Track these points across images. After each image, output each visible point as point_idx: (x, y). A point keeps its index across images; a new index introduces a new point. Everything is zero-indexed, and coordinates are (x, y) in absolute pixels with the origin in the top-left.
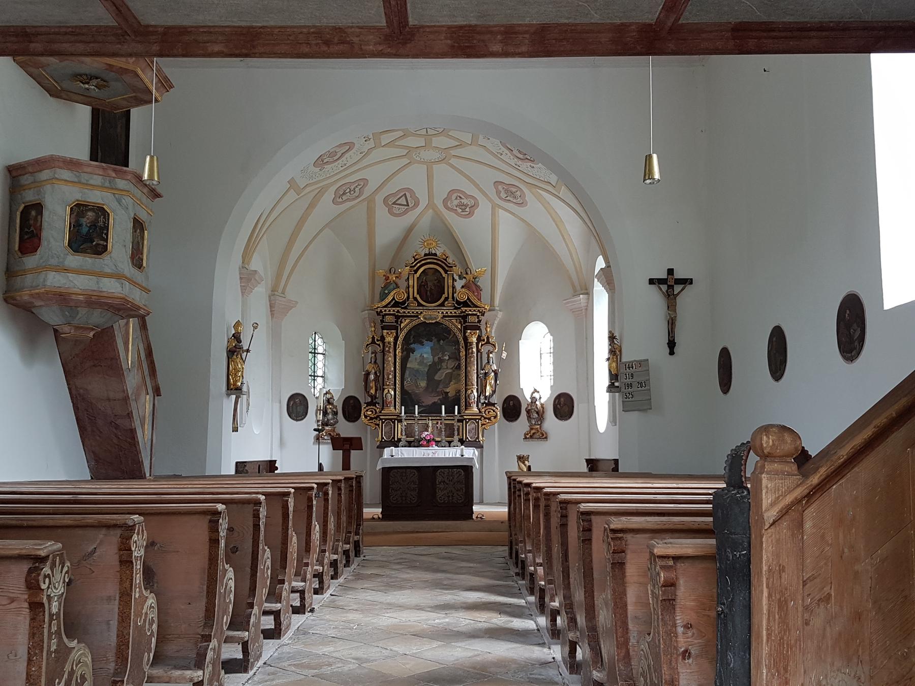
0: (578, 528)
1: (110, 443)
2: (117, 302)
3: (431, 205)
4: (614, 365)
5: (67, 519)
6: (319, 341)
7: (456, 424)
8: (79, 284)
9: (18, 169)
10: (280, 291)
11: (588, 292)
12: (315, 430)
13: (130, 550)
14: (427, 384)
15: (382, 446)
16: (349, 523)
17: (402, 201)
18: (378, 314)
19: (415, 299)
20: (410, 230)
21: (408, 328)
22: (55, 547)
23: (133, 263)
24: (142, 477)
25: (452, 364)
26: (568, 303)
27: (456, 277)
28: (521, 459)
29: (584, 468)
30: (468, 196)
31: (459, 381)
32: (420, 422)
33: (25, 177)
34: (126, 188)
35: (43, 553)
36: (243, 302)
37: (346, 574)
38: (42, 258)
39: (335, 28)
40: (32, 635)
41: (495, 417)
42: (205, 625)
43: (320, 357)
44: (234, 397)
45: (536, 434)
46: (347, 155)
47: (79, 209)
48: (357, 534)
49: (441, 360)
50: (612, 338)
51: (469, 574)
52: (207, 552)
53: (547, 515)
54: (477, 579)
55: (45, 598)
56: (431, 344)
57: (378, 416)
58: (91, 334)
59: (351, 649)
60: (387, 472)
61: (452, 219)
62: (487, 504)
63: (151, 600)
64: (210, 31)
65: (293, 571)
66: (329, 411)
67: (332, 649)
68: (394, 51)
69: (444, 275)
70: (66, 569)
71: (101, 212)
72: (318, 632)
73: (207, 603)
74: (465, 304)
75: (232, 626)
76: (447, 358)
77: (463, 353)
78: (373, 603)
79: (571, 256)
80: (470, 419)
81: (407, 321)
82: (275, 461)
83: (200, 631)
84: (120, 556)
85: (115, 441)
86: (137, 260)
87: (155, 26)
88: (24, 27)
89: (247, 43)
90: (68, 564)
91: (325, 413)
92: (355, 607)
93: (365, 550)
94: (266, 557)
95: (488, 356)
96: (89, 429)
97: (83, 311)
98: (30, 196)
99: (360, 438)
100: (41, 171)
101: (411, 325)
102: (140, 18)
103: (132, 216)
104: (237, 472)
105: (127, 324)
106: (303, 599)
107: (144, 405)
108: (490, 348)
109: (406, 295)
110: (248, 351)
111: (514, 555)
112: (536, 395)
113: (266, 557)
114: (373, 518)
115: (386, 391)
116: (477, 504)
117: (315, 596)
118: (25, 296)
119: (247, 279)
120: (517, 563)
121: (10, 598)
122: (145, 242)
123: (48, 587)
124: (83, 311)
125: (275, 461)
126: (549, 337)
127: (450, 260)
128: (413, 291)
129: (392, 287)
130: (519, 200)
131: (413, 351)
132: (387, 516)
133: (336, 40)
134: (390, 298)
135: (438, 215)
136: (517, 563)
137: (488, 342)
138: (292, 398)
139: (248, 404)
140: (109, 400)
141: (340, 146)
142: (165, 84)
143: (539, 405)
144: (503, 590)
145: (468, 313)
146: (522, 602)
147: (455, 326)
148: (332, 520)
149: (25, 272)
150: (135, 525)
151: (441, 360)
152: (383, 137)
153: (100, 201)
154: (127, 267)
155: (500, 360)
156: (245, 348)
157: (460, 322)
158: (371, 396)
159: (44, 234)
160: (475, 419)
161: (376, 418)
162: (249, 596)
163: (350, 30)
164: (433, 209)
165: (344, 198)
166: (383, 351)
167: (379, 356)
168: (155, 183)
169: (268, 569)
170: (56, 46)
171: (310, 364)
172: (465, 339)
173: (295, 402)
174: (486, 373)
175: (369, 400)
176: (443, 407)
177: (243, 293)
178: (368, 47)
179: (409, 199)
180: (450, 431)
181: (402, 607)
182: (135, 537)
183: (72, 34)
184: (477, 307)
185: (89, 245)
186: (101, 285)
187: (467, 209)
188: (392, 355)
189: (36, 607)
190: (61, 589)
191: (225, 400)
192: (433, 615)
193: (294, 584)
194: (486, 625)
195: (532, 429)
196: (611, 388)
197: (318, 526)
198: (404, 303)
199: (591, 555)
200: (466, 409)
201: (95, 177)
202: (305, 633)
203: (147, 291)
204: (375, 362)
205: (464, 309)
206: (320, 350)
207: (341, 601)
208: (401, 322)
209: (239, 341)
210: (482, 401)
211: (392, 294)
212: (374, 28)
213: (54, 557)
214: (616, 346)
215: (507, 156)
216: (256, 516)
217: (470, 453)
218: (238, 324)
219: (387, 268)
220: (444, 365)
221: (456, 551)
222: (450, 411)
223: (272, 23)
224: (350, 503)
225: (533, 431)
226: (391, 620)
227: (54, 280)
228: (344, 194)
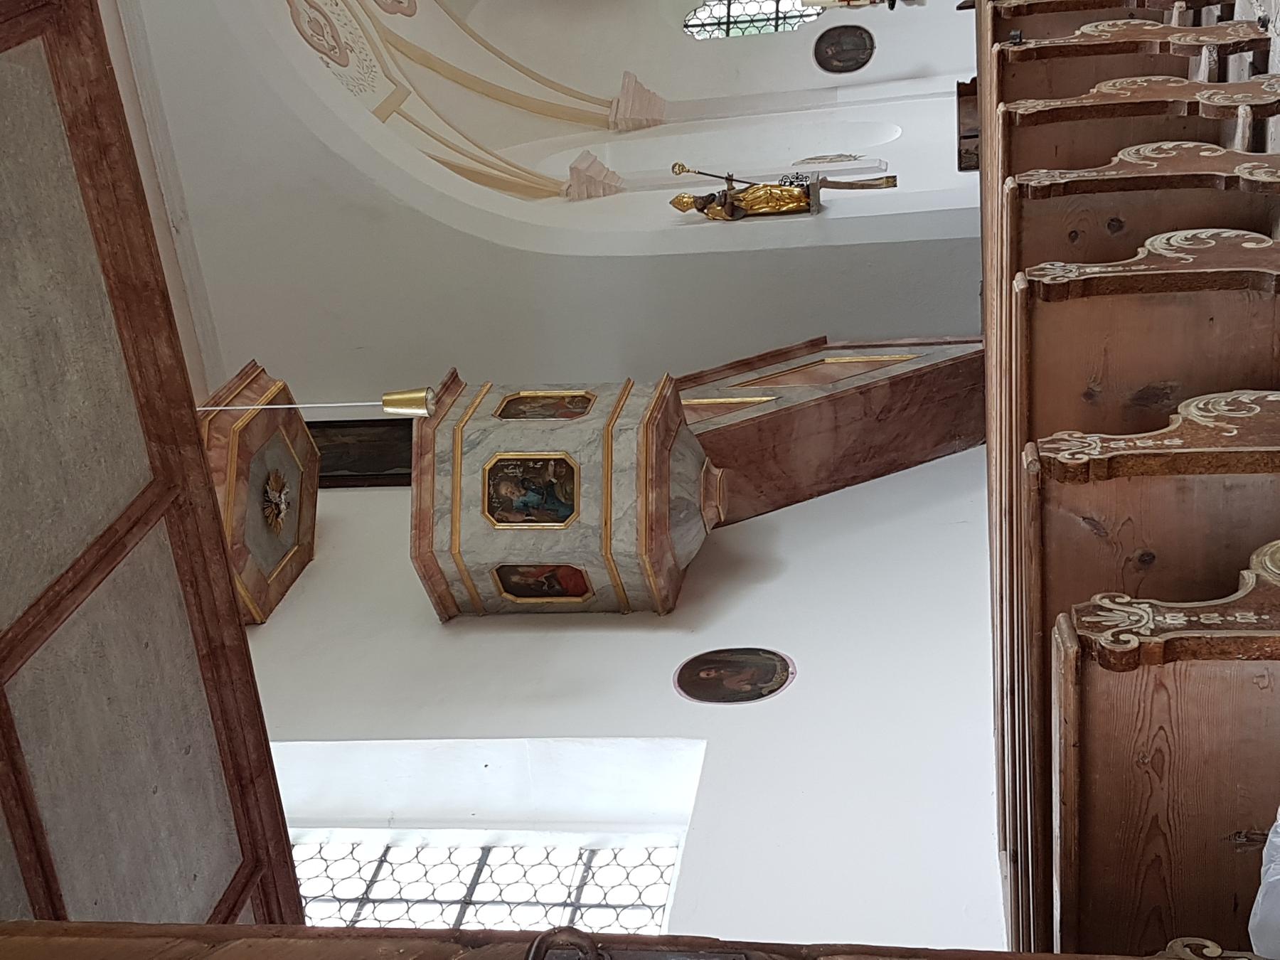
1: (920, 417)
2: (653, 438)
5: (1029, 568)
6: (703, 15)
8: (628, 501)
9: (445, 608)
10: (604, 111)
13: (1087, 464)
22: (1064, 626)
23: (582, 414)
24: (981, 357)
33: (456, 594)
34: (449, 435)
35: (1073, 648)
38: (591, 562)
39: (72, 138)
40: (1225, 654)
42: (1257, 287)
43: (736, 10)
44: (825, 194)
47: (497, 508)
55: (1157, 639)
58: (717, 472)
63: (1191, 410)
64: (137, 363)
65: (1174, 82)
68: (86, 12)
70: (1106, 603)
71: (497, 473)
73: (1211, 287)
82: (959, 85)
83: (1267, 297)
84: (1099, 478)
85: (913, 410)
86: (576, 407)
87: (151, 457)
88: (201, 658)
89: (141, 298)
90: (1097, 599)
94: (1137, 157)
96: (893, 455)
97: (676, 491)
98: (488, 586)
100: (441, 572)
102: (143, 484)
103: (497, 420)
104: (976, 168)
105: (693, 408)
106: (1238, 47)
107: (847, 368)
110: (729, 179)
117: (1237, 17)
118: (659, 584)
119: (589, 184)
121: (1156, 690)
122: (541, 394)
123: (1137, 634)
124: (676, 491)
125: (959, 85)
133: (93, 133)
138: (825, 62)
139: (841, 157)
140: (836, 428)
142: (252, 376)
149: (618, 586)
150: (1040, 459)
153: (479, 476)
154: (592, 422)
159: (549, 561)
162: (1213, 186)
163: (68, 107)
168: (430, 395)
169: (1159, 150)
170: (223, 608)
171: (754, 31)
173: (834, 56)
177: (618, 190)
178: (92, 68)
182: (1064, 457)
183: (195, 584)
185: (557, 489)
186: (627, 464)
189: (1171, 652)
190: (1144, 610)
191: (831, 214)
193: (1202, 75)
197: (1086, 29)
201: (437, 487)
203: (628, 385)
206: (720, 11)
209: (712, 198)
212: (51, 59)
213: (1082, 625)
218: (678, 203)
223: (94, 257)
227: (627, 540)
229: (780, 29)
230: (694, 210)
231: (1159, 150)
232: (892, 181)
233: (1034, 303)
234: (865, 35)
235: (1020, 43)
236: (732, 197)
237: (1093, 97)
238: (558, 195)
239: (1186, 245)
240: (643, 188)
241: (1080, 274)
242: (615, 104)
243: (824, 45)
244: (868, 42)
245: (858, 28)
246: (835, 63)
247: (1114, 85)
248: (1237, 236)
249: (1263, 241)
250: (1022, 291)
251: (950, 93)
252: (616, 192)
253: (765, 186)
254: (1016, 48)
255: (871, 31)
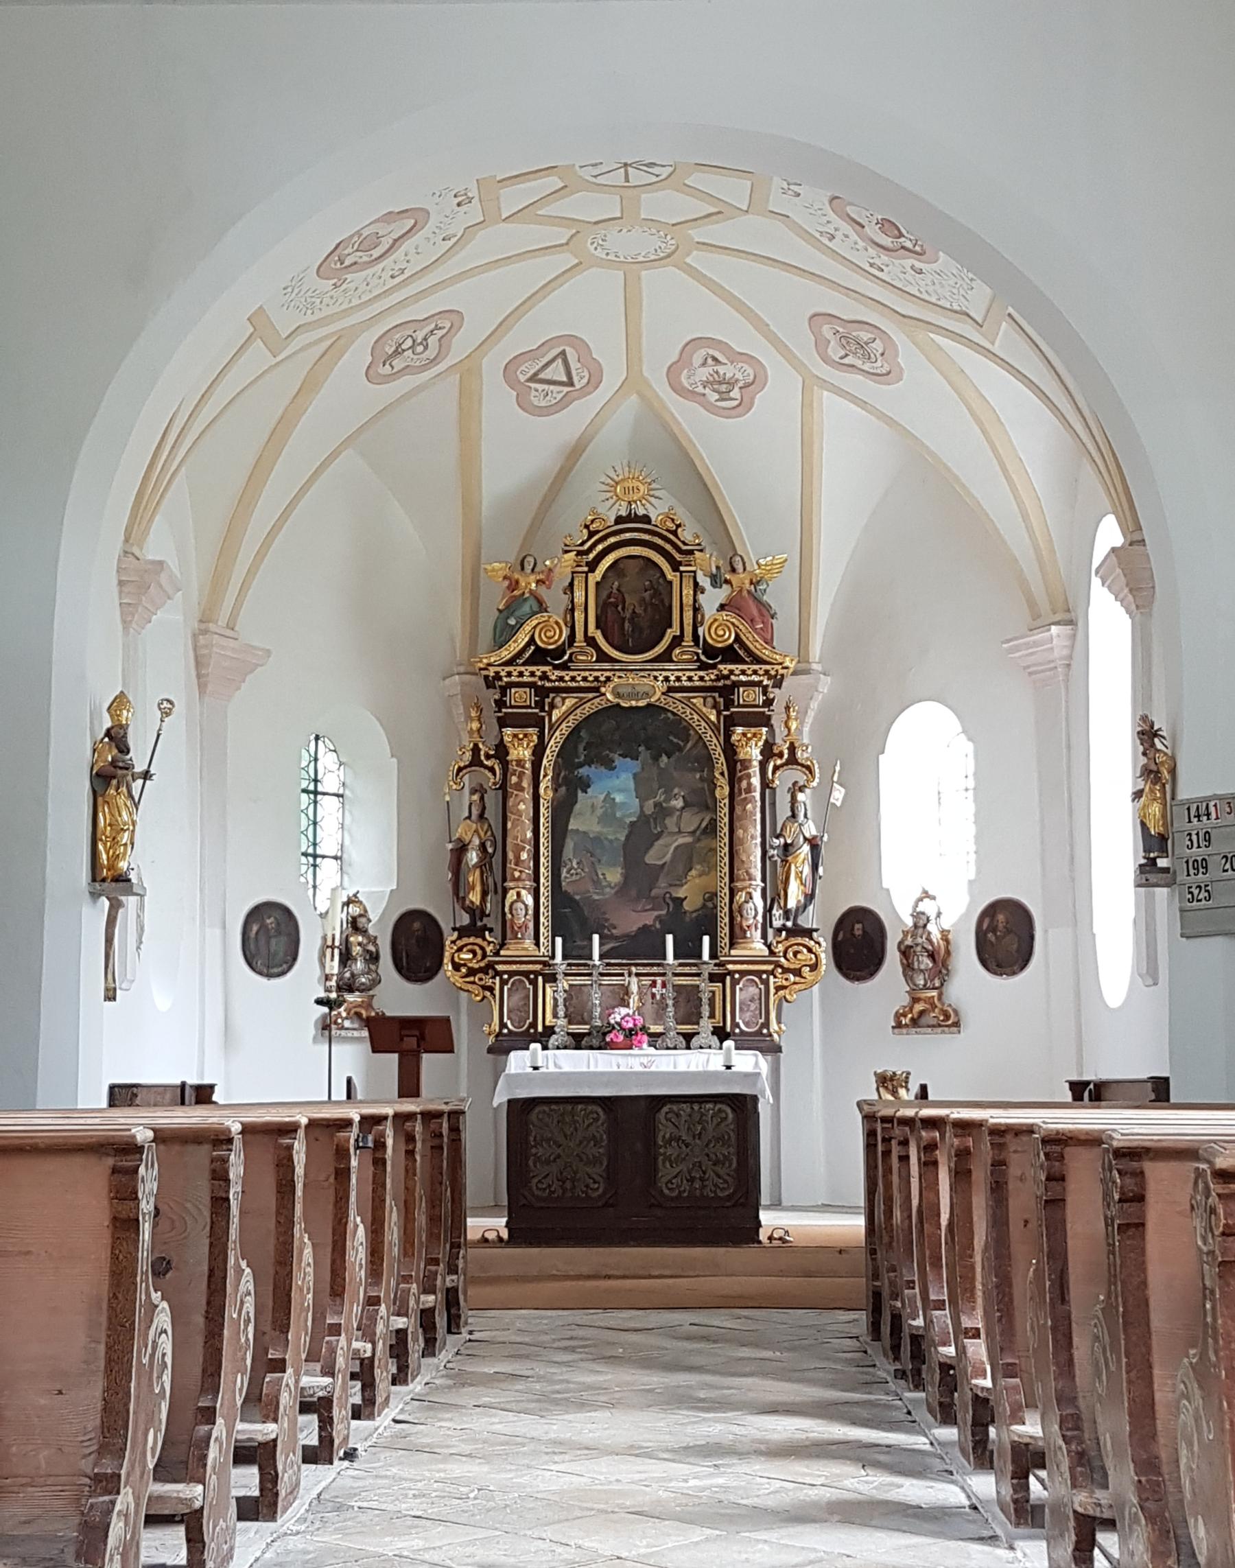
0: (1107, 1195)
3: (633, 381)
4: (1156, 809)
6: (328, 760)
7: (706, 987)
11: (1070, 615)
12: (319, 1002)
14: (626, 877)
15: (503, 1046)
16: (433, 1236)
17: (555, 373)
18: (489, 683)
19: (591, 641)
20: (576, 452)
21: (571, 722)
25: (692, 821)
26: (1017, 649)
27: (704, 581)
28: (886, 1081)
29: (1068, 1097)
30: (737, 357)
31: (712, 867)
32: (606, 981)
36: (126, 647)
37: (428, 1373)
41: (814, 967)
42: (103, 1450)
43: (328, 806)
45: (928, 1014)
46: (408, 245)
48: (452, 1269)
49: (662, 811)
50: (1147, 735)
51: (764, 1374)
52: (105, 1255)
53: (998, 1189)
54: (788, 1386)
56: (635, 766)
57: (491, 966)
59: (472, 1543)
60: (520, 1110)
61: (690, 419)
62: (794, 1208)
66: (356, 950)
67: (418, 1543)
69: (670, 575)
72: (374, 1505)
73: (107, 1390)
74: (729, 654)
75: (163, 1472)
76: (679, 803)
77: (722, 791)
78: (513, 1440)
79: (1025, 517)
80: (743, 973)
81: (569, 702)
82: (211, 1087)
83: (86, 1465)
91: (346, 958)
92: (467, 1449)
93: (473, 1320)
94: (244, 1288)
95: (794, 800)
99: (447, 1020)
101: (579, 715)
106: (326, 1423)
108: (799, 776)
109: (566, 632)
110: (146, 775)
111: (886, 1329)
112: (927, 907)
113: (244, 1288)
114: (485, 1240)
115: (511, 896)
116: (768, 1208)
117: (355, 1423)
119: (138, 584)
120: (896, 1348)
125: (211, 1087)
126: (969, 747)
127: (686, 535)
128: (587, 622)
129: (526, 608)
130: (880, 366)
131: (585, 785)
132: (519, 1234)
134: (522, 639)
135: (653, 414)
136: (896, 1348)
137: (793, 760)
138: (258, 913)
141: (389, 217)
143: (936, 936)
144: (865, 1413)
145: (736, 675)
146: (919, 1442)
147: (702, 714)
148: (393, 1217)
151: (662, 811)
152: (505, 192)
155: (826, 809)
156: (139, 768)
157: (715, 706)
158: (471, 910)
160: (758, 973)
161: (484, 970)
162: (203, 1391)
164: (641, 396)
165: (398, 363)
166: (503, 786)
167: (492, 799)
169: (248, 1321)
172: (730, 751)
173: (263, 926)
174: (786, 846)
175: (465, 919)
176: (670, 938)
177: (126, 624)
179: (574, 365)
180: (689, 1006)
181: (592, 1450)
184: (759, 660)
187: (732, 391)
188: (527, 796)
191: (87, 910)
192: (682, 1469)
194: (828, 1494)
195: (915, 1000)
196: (1148, 872)
197: (361, 1229)
198: (559, 652)
199: (1142, 1267)
200: (732, 945)
202: (339, 1508)
204: (481, 816)
205: (725, 668)
206: (330, 783)
207: (425, 1434)
208: (552, 706)
210: (777, 923)
211: (527, 628)
214: (1160, 758)
215: (848, 242)
216: (220, 1176)
217: (747, 1061)
218: (120, 702)
219: (513, 557)
220: (670, 822)
221: (720, 1320)
222: (689, 950)
224: (434, 1183)
225: (919, 1007)
226: (568, 1478)
228: (398, 352)
229: (304, 859)
230: (108, 723)
231: (248, 1321)
232: (110, 996)
233: (108, 1155)
234: (285, 966)
235: (357, 1147)
236: (125, 776)
237: (302, 1237)
238: (127, 540)
239: (158, 1354)
240: (126, 658)
241: (144, 1214)
242: (229, 633)
243: (278, 914)
244: (276, 970)
245: (295, 959)
246: (255, 928)
247: (309, 1264)
248: (160, 1421)
249: (153, 1457)
250: (134, 1137)
251: (201, 1075)
252: (124, 622)
253: (134, 823)
254: (352, 1141)
255: (289, 975)
